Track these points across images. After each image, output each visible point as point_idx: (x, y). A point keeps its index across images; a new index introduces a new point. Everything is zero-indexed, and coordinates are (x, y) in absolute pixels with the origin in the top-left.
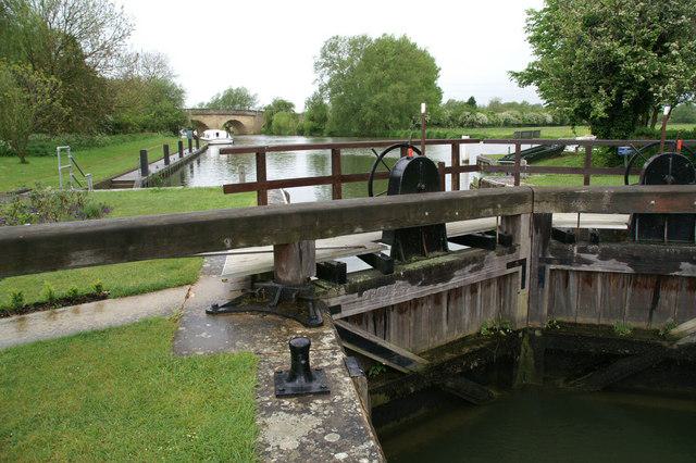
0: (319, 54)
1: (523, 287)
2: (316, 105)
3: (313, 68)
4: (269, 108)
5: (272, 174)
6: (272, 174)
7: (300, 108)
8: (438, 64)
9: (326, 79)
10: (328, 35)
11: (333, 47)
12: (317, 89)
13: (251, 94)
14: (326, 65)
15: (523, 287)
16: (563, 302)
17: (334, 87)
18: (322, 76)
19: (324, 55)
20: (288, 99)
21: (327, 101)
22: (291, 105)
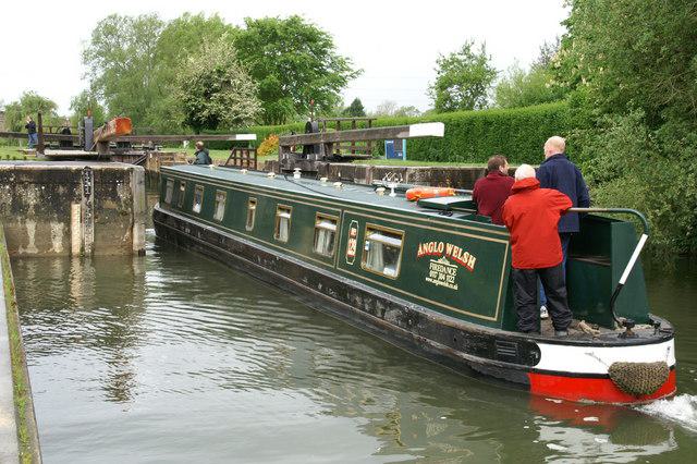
0: (90, 39)
1: (563, 433)
2: (86, 107)
3: (80, 58)
4: (15, 107)
5: (365, 144)
6: (365, 144)
7: (65, 111)
8: (341, 48)
9: (100, 73)
10: (100, 14)
11: (110, 31)
12: (86, 85)
13: (293, 15)
14: (100, 53)
15: (563, 433)
16: (413, 450)
17: (110, 83)
18: (94, 69)
19: (96, 41)
20: (45, 94)
21: (101, 103)
22: (51, 105)
